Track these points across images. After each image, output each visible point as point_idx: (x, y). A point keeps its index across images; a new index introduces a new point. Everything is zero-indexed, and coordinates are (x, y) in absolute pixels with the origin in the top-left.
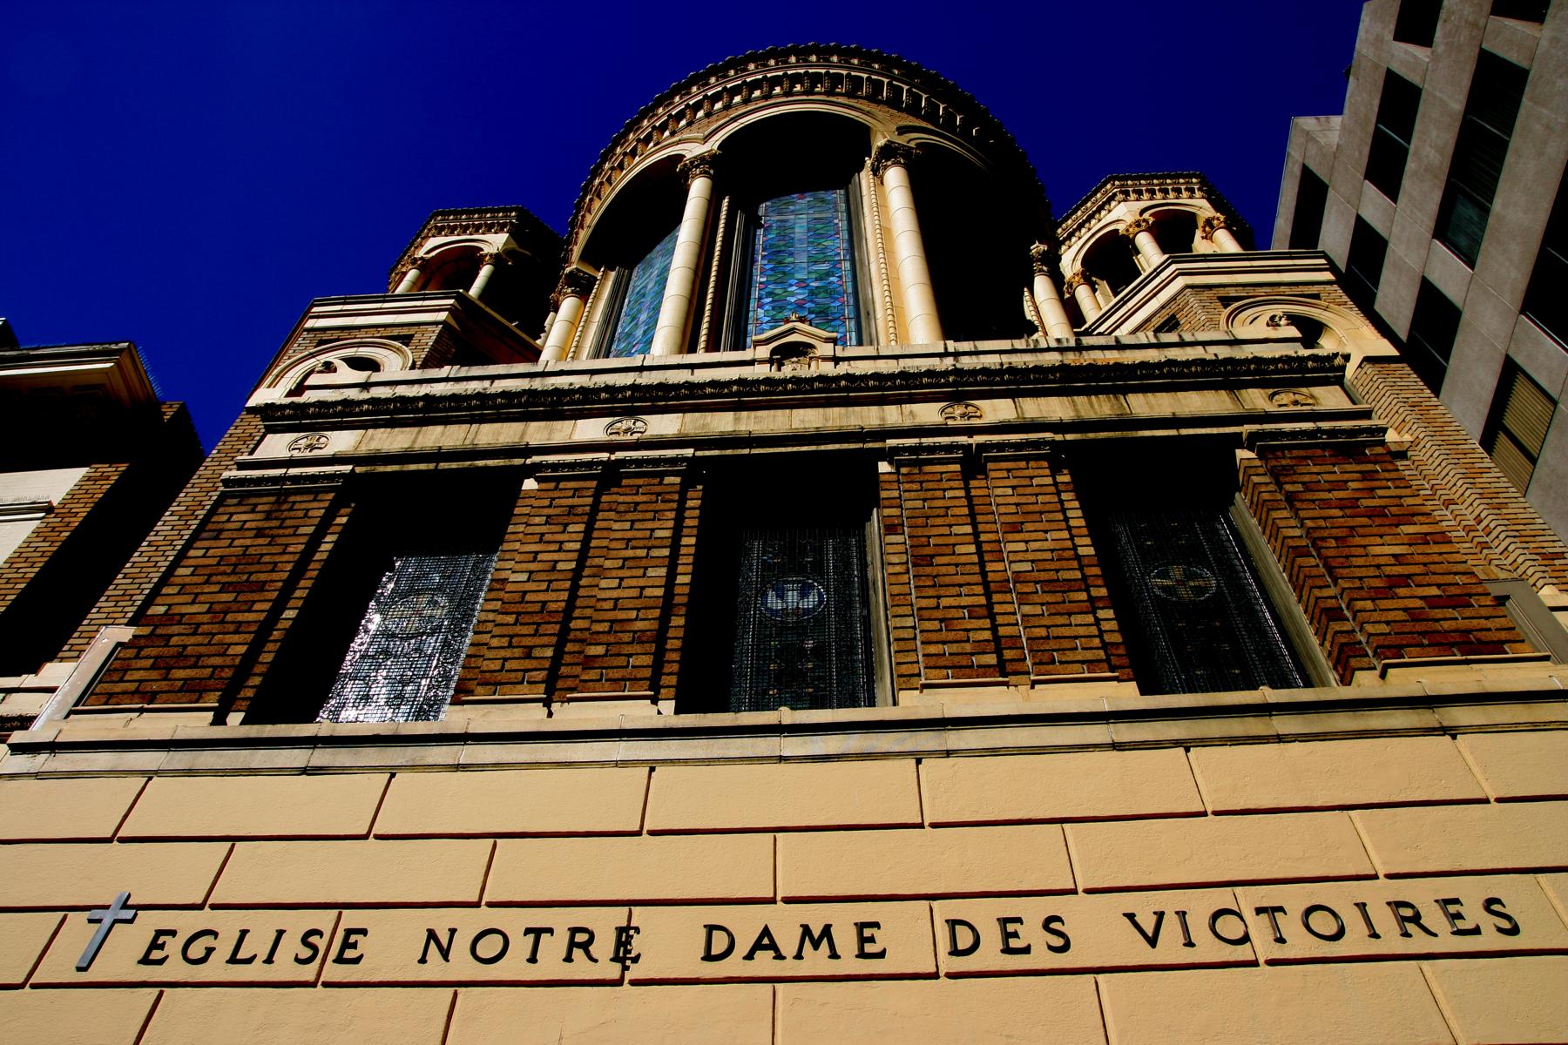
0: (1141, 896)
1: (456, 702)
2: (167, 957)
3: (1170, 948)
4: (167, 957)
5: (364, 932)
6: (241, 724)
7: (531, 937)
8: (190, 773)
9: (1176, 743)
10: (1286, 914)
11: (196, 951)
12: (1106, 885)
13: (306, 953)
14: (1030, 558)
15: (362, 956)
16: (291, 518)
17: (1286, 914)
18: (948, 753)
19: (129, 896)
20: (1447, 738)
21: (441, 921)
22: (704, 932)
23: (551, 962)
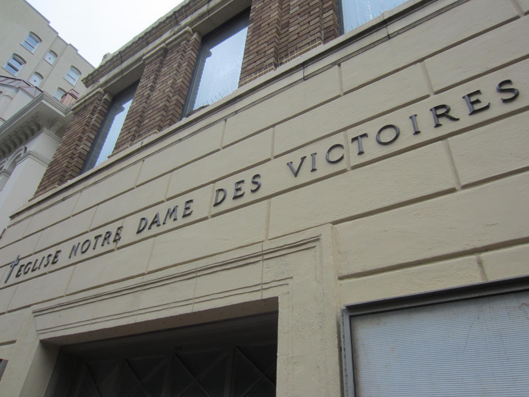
0: (361, 126)
1: (131, 146)
2: (192, 211)
3: (305, 175)
4: (192, 211)
5: (191, 201)
6: (238, 88)
7: (356, 142)
8: (41, 211)
9: (333, 64)
10: (177, 206)
11: (221, 195)
12: (283, 152)
13: (255, 187)
14: (132, 119)
15: (244, 193)
16: (187, 55)
17: (177, 206)
18: (236, 112)
19: (19, 256)
20: (337, 66)
21: (219, 185)
22: (288, 167)
23: (324, 169)
